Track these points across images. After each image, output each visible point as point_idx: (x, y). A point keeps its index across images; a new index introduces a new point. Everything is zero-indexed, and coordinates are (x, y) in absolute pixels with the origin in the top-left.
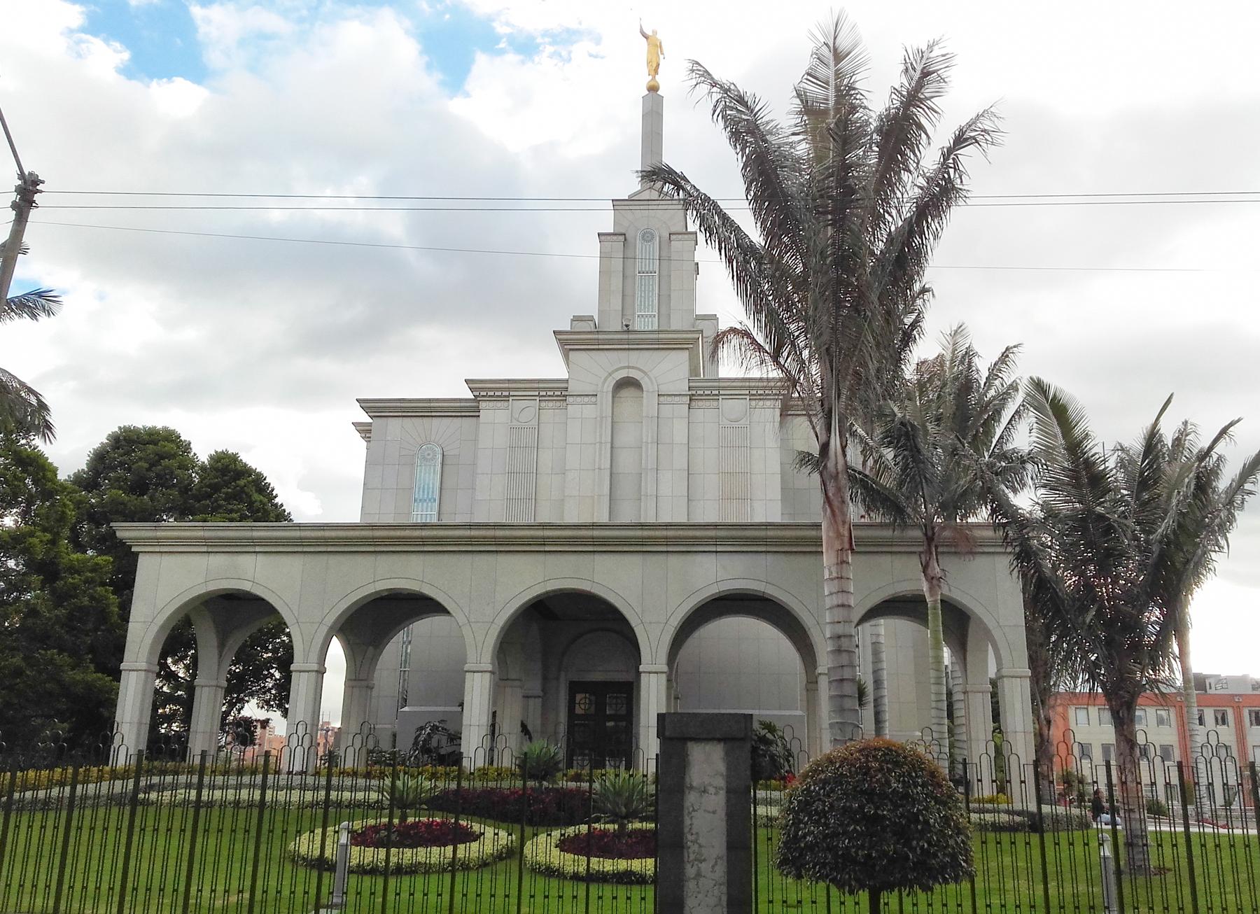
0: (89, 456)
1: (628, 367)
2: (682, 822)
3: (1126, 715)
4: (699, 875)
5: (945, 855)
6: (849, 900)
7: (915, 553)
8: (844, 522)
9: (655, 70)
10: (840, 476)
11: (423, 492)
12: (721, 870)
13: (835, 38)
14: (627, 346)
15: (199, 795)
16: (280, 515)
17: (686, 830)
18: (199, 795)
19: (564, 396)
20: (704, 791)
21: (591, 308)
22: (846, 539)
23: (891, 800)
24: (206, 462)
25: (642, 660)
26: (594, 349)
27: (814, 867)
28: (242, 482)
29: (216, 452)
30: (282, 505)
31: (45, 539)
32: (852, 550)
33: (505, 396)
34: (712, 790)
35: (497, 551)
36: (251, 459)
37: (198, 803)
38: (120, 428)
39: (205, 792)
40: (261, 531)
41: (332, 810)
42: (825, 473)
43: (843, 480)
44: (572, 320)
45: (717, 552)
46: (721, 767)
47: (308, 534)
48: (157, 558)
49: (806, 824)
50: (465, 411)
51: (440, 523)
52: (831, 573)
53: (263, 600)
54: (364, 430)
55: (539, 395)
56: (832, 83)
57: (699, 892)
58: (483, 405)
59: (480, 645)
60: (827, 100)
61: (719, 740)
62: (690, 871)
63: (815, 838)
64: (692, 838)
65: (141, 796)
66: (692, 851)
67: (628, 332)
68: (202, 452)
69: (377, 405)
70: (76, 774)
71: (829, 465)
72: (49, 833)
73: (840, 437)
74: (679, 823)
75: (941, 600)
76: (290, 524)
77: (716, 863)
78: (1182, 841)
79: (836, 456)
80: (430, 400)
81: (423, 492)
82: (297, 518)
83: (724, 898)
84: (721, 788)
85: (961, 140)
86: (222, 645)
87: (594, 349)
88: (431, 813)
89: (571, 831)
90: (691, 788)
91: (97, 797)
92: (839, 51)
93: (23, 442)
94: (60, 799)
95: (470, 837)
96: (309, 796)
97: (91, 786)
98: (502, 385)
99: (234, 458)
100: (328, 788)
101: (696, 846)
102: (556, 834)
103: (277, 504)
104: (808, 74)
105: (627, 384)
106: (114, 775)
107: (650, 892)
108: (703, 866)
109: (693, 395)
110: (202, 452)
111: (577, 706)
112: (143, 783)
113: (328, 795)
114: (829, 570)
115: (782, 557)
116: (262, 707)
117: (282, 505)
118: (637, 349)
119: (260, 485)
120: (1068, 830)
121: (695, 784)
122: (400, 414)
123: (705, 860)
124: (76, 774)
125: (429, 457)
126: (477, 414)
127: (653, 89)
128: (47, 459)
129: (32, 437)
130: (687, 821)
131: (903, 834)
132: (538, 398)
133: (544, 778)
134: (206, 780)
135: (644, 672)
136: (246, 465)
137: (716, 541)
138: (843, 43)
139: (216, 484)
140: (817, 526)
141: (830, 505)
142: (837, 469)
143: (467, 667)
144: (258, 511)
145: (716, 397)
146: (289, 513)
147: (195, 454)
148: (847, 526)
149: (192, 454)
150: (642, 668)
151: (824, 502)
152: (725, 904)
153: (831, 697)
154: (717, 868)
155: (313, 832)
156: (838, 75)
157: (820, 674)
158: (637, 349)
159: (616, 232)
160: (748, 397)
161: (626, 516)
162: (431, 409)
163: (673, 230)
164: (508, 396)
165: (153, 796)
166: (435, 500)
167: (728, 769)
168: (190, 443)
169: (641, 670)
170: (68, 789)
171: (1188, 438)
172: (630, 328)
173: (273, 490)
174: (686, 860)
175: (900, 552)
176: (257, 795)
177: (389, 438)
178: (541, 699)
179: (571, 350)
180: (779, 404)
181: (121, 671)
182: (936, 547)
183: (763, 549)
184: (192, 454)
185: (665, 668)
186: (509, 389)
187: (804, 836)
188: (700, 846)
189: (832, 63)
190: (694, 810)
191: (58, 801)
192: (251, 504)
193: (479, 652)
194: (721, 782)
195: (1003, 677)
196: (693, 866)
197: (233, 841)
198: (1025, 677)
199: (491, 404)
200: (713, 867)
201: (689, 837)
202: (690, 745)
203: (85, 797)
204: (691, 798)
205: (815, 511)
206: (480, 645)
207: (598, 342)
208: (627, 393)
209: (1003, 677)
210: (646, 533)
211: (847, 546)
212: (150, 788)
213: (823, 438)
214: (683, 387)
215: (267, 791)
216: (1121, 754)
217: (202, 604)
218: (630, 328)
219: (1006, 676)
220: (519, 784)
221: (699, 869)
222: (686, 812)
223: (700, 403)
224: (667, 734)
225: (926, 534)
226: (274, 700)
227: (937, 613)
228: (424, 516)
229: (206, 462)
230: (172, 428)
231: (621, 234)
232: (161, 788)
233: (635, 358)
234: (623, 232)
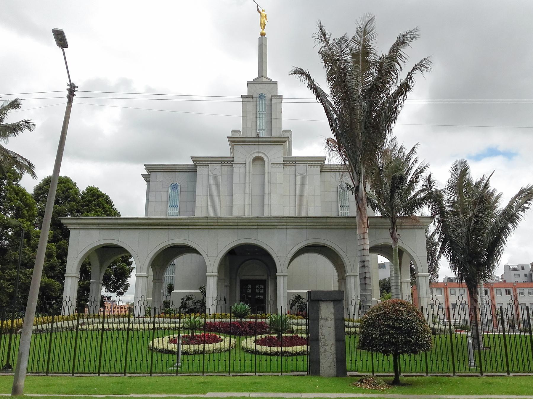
0: (34, 188)
1: (259, 152)
2: (318, 331)
3: (474, 290)
4: (325, 351)
5: (424, 341)
6: (386, 357)
7: (387, 228)
8: (365, 217)
9: (263, 26)
10: (364, 199)
11: (173, 203)
12: (333, 348)
13: (366, 26)
14: (270, 143)
15: (103, 326)
16: (116, 214)
17: (320, 334)
18: (103, 326)
19: (232, 164)
20: (327, 320)
21: (238, 125)
22: (366, 224)
23: (404, 321)
24: (85, 191)
25: (278, 270)
26: (251, 145)
27: (376, 346)
28: (100, 199)
29: (89, 187)
30: (116, 209)
31: (28, 224)
32: (368, 228)
33: (207, 164)
34: (329, 319)
35: (218, 228)
36: (103, 190)
37: (103, 329)
38: (47, 176)
39: (105, 325)
40: (105, 219)
41: (156, 331)
42: (357, 198)
43: (365, 200)
44: (231, 132)
45: (306, 228)
46: (332, 310)
47: (142, 221)
48: (78, 231)
49: (372, 330)
50: (192, 170)
51: (147, 217)
52: (360, 237)
53: (123, 248)
54: (147, 178)
55: (308, 164)
56: (362, 43)
57: (326, 357)
58: (198, 167)
59: (212, 265)
60: (359, 50)
61: (332, 301)
62: (322, 349)
63: (376, 336)
64: (323, 337)
65: (80, 327)
66: (322, 342)
67: (258, 137)
68: (82, 187)
69: (151, 167)
70: (53, 319)
71: (359, 195)
72: (69, 340)
73: (364, 184)
74: (318, 332)
75: (398, 248)
76: (119, 217)
77: (332, 346)
78: (502, 337)
79: (362, 191)
80: (175, 165)
81: (173, 203)
82: (124, 214)
83: (335, 359)
84: (333, 318)
85: (419, 67)
86: (101, 266)
87: (251, 145)
88: (200, 331)
89: (258, 337)
90: (322, 318)
91: (62, 328)
92: (366, 31)
93: (14, 183)
94: (47, 329)
95: (219, 340)
96: (147, 326)
97: (60, 323)
98: (206, 159)
99: (97, 189)
100: (154, 323)
101: (324, 340)
102: (254, 338)
103: (114, 208)
104: (353, 39)
105: (258, 159)
106: (64, 319)
107: (305, 357)
108: (327, 347)
109: (285, 164)
110: (82, 187)
111: (263, 287)
112: (80, 322)
113: (154, 325)
114: (360, 236)
115: (314, 230)
116: (107, 292)
117: (116, 209)
118: (262, 145)
119: (107, 200)
120: (509, 320)
121: (323, 317)
122: (162, 171)
123: (327, 345)
124: (53, 319)
125: (175, 189)
126: (196, 171)
127: (263, 35)
128: (26, 190)
129: (18, 181)
130: (320, 331)
131: (409, 333)
132: (221, 164)
133: (243, 317)
134: (106, 320)
135: (278, 276)
136: (101, 192)
137: (287, 224)
138: (369, 28)
139: (90, 200)
140: (355, 218)
141: (360, 211)
142: (362, 196)
143: (207, 274)
144: (107, 211)
145: (294, 165)
146: (119, 212)
147: (78, 188)
148: (366, 219)
149: (77, 187)
150: (348, 273)
151: (357, 209)
152: (335, 361)
153: (360, 284)
154: (332, 348)
155: (164, 338)
156: (364, 40)
157: (348, 276)
158: (262, 145)
159: (249, 95)
160: (307, 164)
161: (236, 214)
162: (175, 169)
163: (272, 94)
164: (295, 163)
165: (85, 327)
166: (178, 206)
167: (335, 311)
168: (76, 183)
169: (277, 275)
170: (50, 324)
171: (483, 182)
172: (260, 136)
173: (112, 202)
174: (320, 345)
175: (331, 228)
176: (126, 326)
177: (158, 181)
178: (229, 287)
179: (234, 145)
180: (319, 167)
181: (65, 277)
182: (396, 226)
183: (78, 228)
184: (77, 187)
185: (216, 274)
186: (209, 161)
187: (372, 335)
188: (326, 340)
189: (362, 35)
190: (323, 327)
191: (46, 330)
192: (104, 208)
193: (212, 267)
194: (332, 316)
195: (419, 276)
196: (323, 348)
197: (138, 342)
198: (215, 276)
199: (202, 167)
200: (331, 348)
201: (321, 337)
202: (320, 302)
203: (57, 328)
204: (321, 322)
205: (352, 211)
206: (212, 265)
207: (246, 142)
208: (258, 163)
209: (419, 276)
210: (278, 221)
211: (366, 226)
212: (83, 324)
213: (356, 184)
214: (281, 160)
215: (130, 324)
216: (472, 305)
217: (95, 250)
218: (260, 136)
219: (420, 276)
220: (228, 320)
221: (325, 348)
222: (320, 327)
223: (288, 167)
224: (312, 298)
225: (392, 221)
226: (112, 289)
227: (396, 252)
228: (171, 213)
229: (85, 191)
230: (68, 176)
231: (251, 96)
232: (88, 324)
233: (261, 148)
234: (252, 95)
